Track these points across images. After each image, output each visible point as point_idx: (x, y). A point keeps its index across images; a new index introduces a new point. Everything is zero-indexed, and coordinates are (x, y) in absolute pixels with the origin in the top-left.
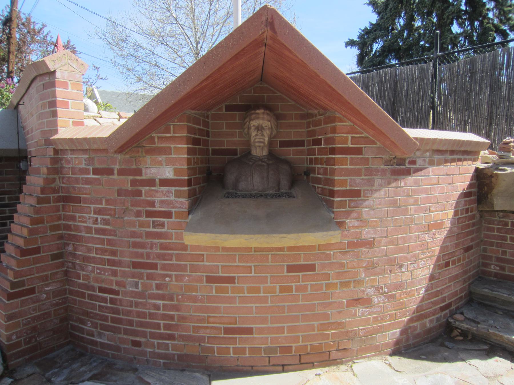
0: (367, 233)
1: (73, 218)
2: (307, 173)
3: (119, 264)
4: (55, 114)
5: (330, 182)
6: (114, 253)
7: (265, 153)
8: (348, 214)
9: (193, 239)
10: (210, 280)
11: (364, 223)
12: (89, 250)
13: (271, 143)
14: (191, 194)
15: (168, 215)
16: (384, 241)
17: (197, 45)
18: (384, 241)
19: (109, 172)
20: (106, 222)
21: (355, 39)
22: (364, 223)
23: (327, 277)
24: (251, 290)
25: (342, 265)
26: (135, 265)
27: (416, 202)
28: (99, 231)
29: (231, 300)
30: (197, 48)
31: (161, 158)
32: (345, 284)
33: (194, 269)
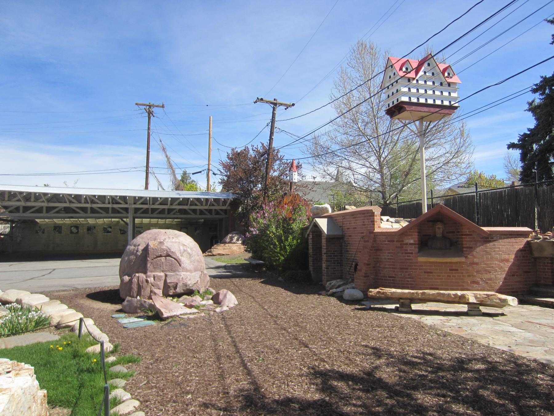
0: (476, 260)
1: (380, 255)
2: (456, 242)
3: (396, 268)
4: (374, 224)
5: (462, 244)
6: (394, 265)
7: (441, 235)
8: (468, 254)
9: (421, 259)
10: (425, 272)
11: (475, 257)
12: (385, 265)
13: (443, 232)
14: (419, 248)
15: (412, 253)
16: (482, 263)
17: (380, 150)
18: (482, 263)
19: (393, 241)
20: (392, 256)
21: (516, 142)
22: (475, 257)
23: (462, 273)
24: (438, 276)
25: (467, 270)
26: (401, 269)
27: (495, 251)
28: (389, 259)
29: (432, 279)
30: (379, 152)
31: (410, 237)
32: (469, 276)
33: (420, 269)
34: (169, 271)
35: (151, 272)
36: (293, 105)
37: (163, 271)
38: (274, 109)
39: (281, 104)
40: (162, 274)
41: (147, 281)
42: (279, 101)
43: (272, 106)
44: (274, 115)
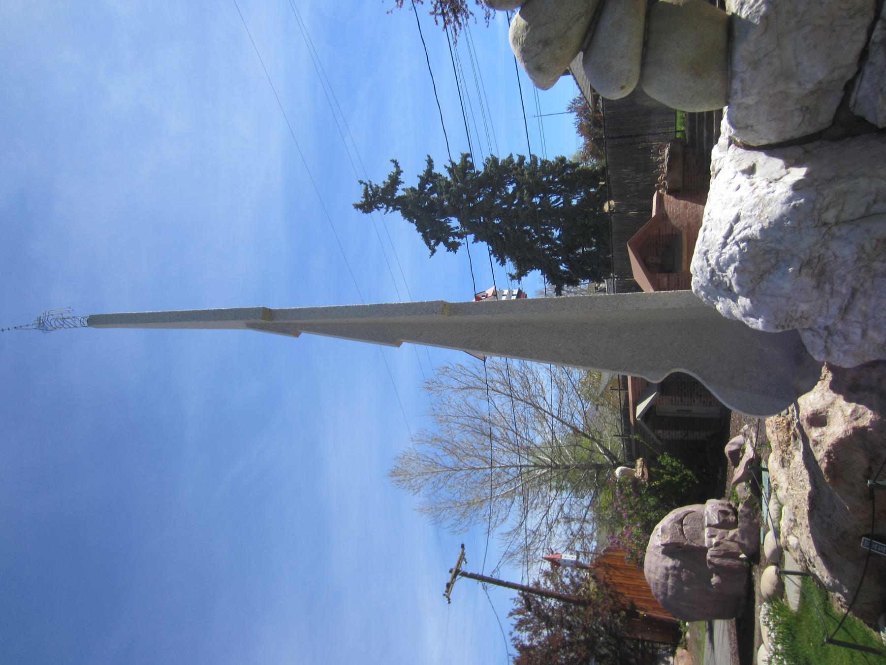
0: (685, 224)
34: (703, 523)
35: (704, 542)
36: (463, 546)
37: (703, 529)
38: (464, 574)
39: (459, 564)
40: (707, 530)
41: (717, 544)
42: (453, 566)
43: (458, 577)
44: (472, 576)
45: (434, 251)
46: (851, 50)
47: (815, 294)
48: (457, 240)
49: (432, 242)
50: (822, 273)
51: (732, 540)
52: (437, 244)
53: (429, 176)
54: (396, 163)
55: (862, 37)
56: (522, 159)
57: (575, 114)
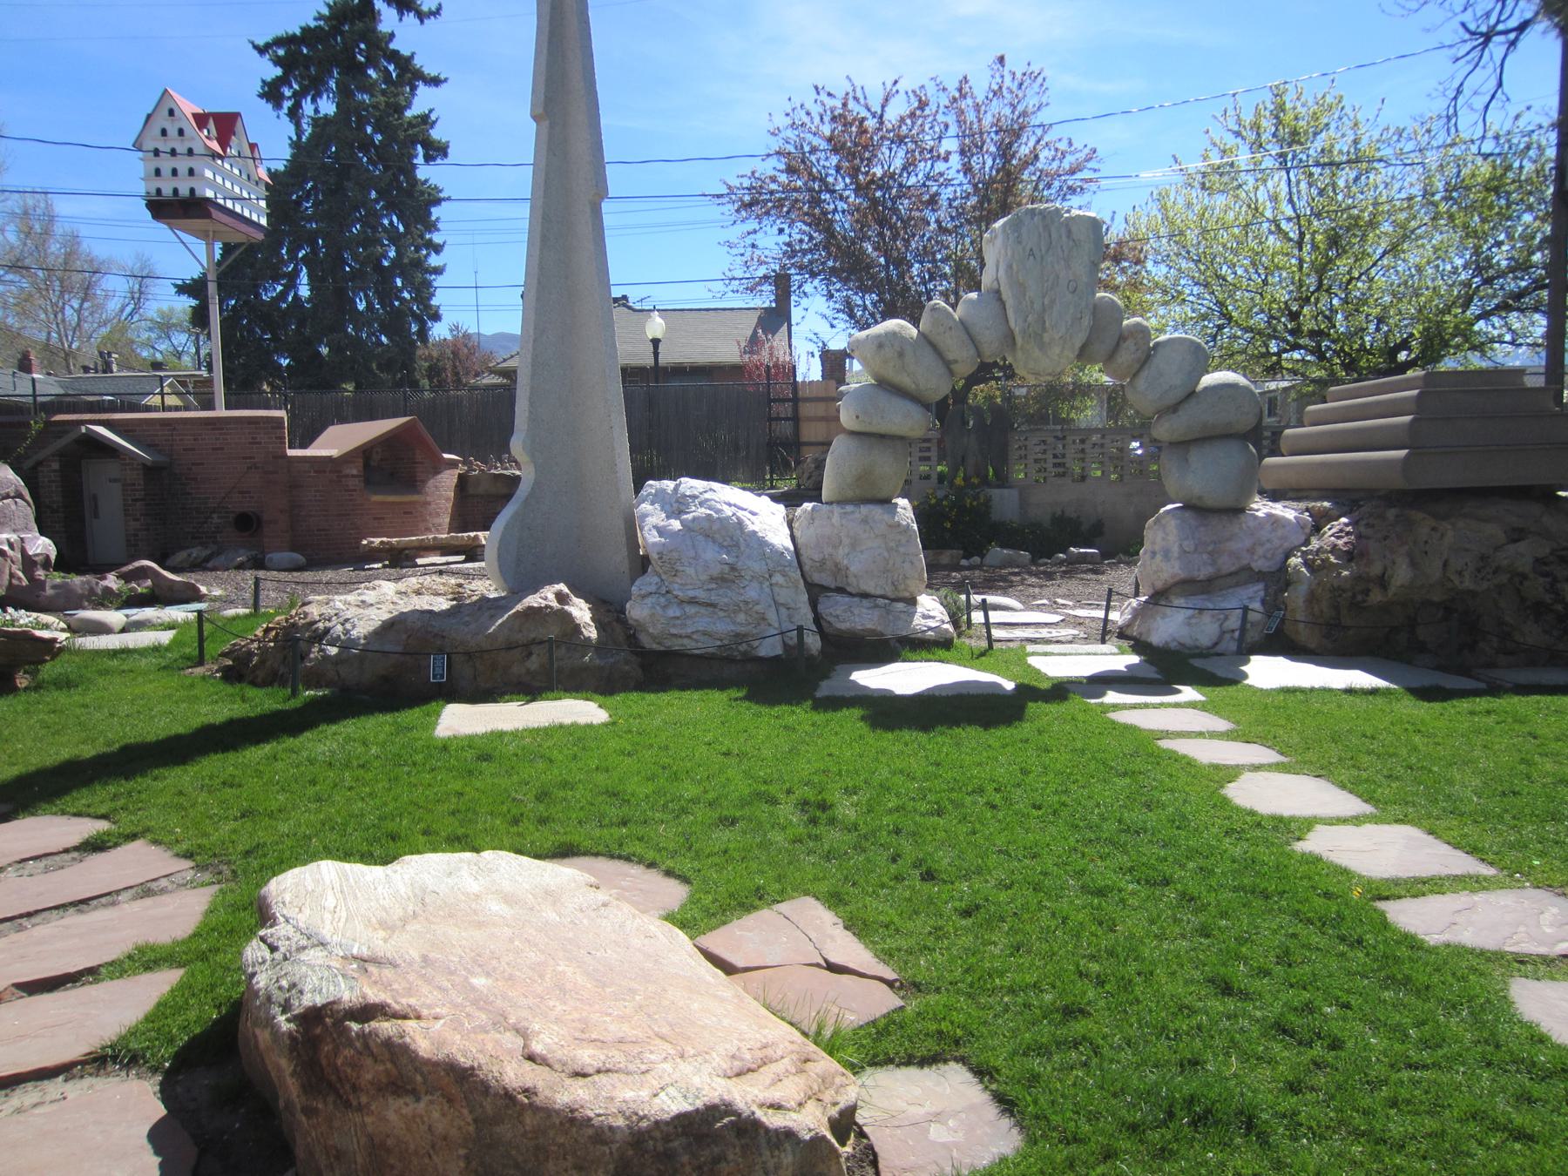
34: (22, 530)
45: (262, 50)
46: (869, 587)
47: (704, 577)
48: (287, 104)
49: (281, 52)
50: (723, 580)
51: (12, 575)
52: (277, 61)
53: (409, 74)
54: (436, 13)
55: (879, 592)
56: (438, 249)
57: (449, 337)
